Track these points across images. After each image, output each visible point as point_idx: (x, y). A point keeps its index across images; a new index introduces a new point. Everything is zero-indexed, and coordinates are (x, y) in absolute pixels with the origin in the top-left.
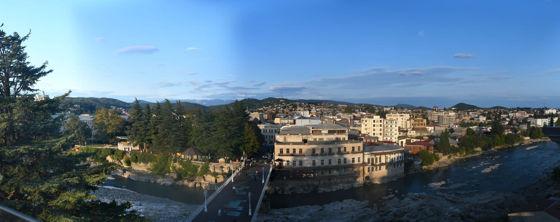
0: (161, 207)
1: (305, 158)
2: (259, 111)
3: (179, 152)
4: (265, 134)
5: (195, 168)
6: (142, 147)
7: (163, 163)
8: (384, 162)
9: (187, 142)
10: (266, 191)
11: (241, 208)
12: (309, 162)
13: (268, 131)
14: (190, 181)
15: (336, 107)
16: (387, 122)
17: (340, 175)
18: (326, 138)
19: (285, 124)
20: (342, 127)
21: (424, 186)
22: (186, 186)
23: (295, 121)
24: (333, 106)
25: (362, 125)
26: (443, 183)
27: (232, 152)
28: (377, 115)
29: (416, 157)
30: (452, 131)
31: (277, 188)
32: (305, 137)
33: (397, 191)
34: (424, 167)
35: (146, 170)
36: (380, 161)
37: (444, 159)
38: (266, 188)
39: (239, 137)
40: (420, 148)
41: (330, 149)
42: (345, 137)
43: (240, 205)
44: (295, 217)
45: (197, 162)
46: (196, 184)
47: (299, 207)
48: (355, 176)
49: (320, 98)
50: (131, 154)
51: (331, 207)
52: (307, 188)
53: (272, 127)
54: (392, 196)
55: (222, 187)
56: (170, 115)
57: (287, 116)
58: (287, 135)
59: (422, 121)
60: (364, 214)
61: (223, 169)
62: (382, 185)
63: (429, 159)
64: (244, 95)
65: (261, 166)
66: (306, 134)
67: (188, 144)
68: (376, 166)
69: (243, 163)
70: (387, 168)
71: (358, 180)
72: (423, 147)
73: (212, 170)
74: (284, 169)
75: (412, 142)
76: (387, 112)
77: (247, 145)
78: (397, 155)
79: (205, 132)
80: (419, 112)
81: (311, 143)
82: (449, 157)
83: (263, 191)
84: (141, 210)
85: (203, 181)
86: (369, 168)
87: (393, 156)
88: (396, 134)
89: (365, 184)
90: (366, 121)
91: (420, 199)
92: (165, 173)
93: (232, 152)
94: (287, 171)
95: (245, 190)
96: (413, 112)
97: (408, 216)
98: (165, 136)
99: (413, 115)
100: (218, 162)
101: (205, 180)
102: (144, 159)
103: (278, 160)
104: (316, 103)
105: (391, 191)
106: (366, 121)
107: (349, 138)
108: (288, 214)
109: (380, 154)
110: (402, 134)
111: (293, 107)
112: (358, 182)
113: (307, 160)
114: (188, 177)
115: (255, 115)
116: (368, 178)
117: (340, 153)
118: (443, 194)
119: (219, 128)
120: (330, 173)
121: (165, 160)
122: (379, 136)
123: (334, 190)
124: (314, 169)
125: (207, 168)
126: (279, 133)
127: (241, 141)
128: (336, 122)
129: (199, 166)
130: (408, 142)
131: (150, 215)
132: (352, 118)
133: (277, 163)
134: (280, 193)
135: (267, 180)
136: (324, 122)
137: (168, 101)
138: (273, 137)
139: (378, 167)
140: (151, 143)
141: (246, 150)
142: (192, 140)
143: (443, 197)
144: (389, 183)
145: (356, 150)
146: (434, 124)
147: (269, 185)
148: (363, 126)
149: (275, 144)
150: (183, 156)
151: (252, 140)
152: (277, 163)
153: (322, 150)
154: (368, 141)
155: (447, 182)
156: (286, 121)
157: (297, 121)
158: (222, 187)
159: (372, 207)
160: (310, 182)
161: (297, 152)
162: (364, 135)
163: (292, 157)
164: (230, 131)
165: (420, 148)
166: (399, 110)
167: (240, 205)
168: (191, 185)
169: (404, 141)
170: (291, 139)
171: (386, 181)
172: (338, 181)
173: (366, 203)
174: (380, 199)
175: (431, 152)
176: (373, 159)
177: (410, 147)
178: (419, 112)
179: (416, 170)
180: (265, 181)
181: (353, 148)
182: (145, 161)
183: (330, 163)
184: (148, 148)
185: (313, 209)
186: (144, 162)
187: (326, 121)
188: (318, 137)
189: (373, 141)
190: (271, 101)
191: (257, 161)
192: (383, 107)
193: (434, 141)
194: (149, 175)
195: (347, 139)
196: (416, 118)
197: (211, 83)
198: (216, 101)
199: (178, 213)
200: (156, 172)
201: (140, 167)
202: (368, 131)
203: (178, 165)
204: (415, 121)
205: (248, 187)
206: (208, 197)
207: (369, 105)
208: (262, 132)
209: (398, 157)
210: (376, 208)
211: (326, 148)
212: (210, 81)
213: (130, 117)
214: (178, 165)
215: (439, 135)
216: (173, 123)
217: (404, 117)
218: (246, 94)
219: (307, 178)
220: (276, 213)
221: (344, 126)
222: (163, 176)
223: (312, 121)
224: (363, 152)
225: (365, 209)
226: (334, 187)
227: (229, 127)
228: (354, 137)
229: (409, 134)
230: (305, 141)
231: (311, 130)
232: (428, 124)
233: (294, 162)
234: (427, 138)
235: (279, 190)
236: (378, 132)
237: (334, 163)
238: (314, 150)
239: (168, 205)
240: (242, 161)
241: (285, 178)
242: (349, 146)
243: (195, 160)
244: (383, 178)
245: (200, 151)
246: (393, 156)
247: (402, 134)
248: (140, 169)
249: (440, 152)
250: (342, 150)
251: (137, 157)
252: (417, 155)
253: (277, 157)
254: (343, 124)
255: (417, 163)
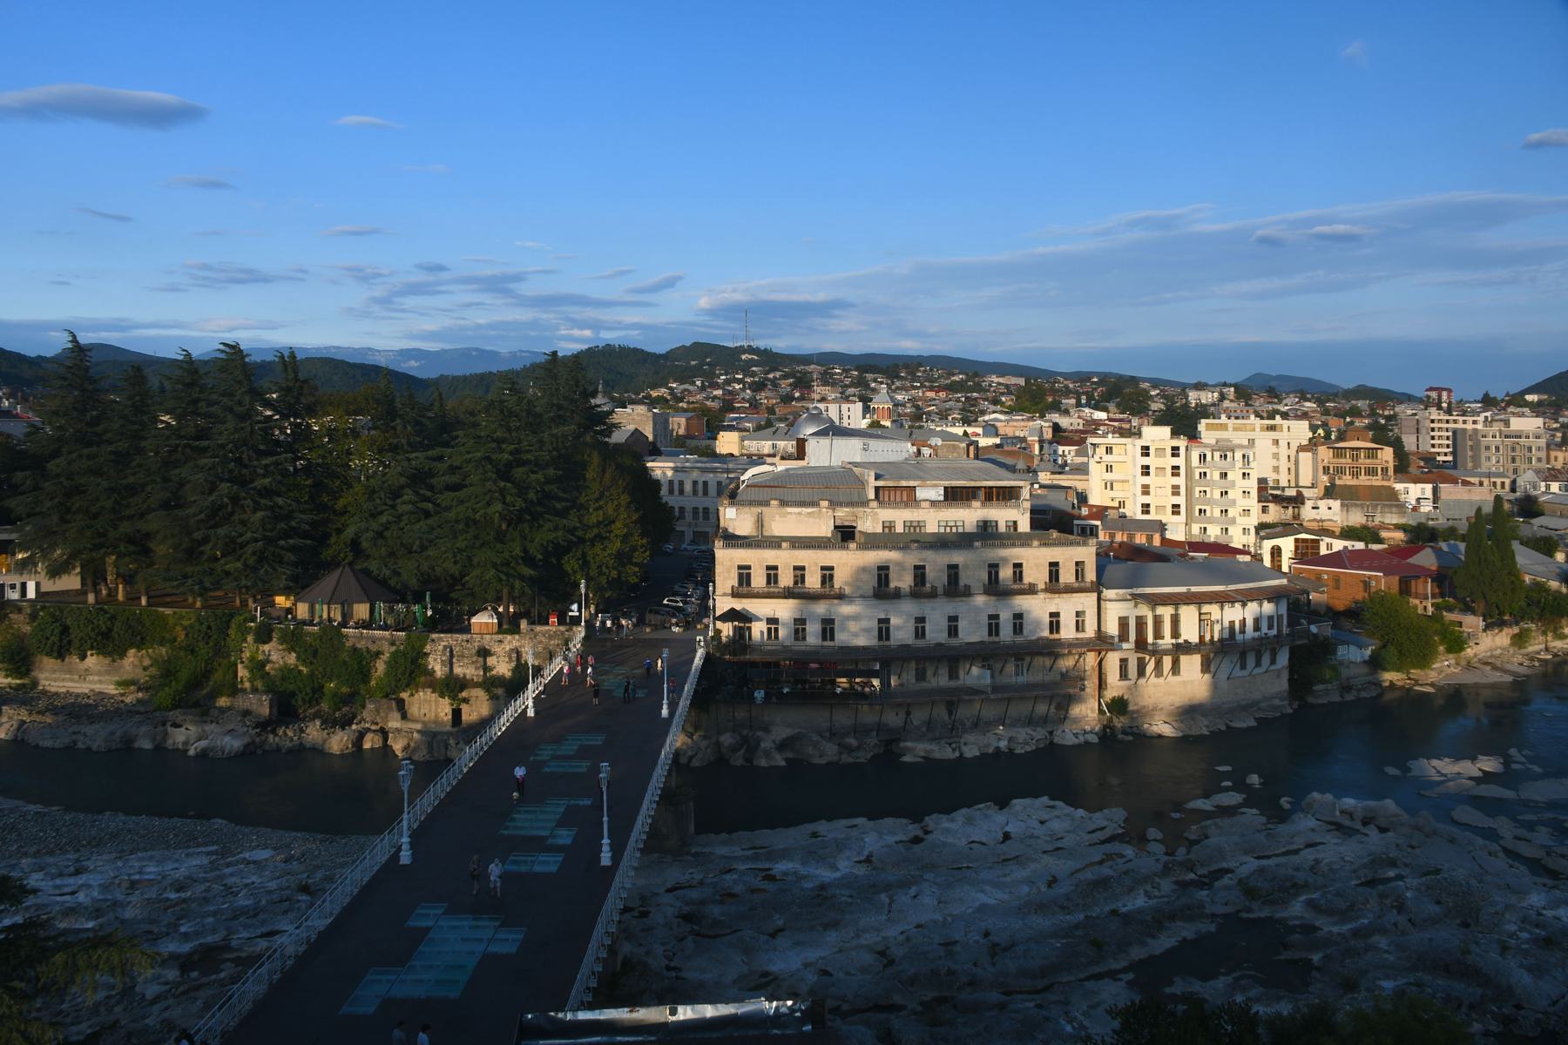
0: (191, 863)
1: (846, 609)
2: (652, 403)
3: (286, 592)
4: (673, 501)
5: (362, 662)
6: (93, 576)
7: (204, 650)
8: (1195, 639)
9: (323, 539)
10: (677, 754)
11: (565, 837)
12: (865, 624)
13: (688, 487)
14: (331, 723)
15: (978, 388)
16: (1203, 458)
17: (996, 688)
18: (934, 520)
19: (759, 459)
20: (1003, 472)
21: (1391, 771)
22: (318, 751)
23: (801, 444)
24: (963, 383)
25: (1093, 466)
26: (1489, 764)
27: (531, 581)
28: (1158, 422)
29: (1347, 624)
30: (1529, 507)
31: (727, 739)
32: (843, 514)
33: (1254, 779)
34: (1389, 677)
35: (111, 689)
36: (1175, 633)
37: (1490, 648)
38: (676, 739)
39: (562, 514)
40: (1366, 584)
41: (953, 569)
42: (1017, 516)
43: (563, 823)
44: (803, 871)
45: (370, 630)
46: (361, 736)
47: (822, 827)
48: (1064, 691)
49: (909, 346)
50: (33, 617)
51: (958, 830)
52: (852, 741)
53: (704, 470)
54: (1232, 798)
55: (482, 742)
56: (246, 416)
57: (769, 424)
58: (766, 504)
59: (1371, 453)
60: (1106, 871)
61: (491, 661)
62: (1184, 742)
63: (1414, 642)
64: (587, 333)
65: (656, 645)
66: (851, 504)
67: (327, 554)
68: (1157, 653)
69: (580, 632)
70: (1206, 667)
71: (1077, 710)
72: (1381, 581)
73: (437, 666)
74: (756, 657)
75: (1323, 551)
76: (1203, 412)
77: (598, 549)
78: (1253, 607)
79: (408, 495)
80: (1357, 411)
81: (872, 542)
82: (1520, 640)
83: (665, 753)
84: (81, 897)
85: (394, 723)
86: (1124, 662)
87: (1234, 614)
88: (1246, 512)
89: (1107, 735)
90: (1109, 450)
91: (1372, 832)
92: (214, 695)
93: (531, 581)
94: (767, 665)
95: (583, 753)
96: (1326, 412)
97: (1311, 904)
98: (216, 516)
99: (1325, 425)
100: (467, 630)
101: (404, 717)
102: (106, 635)
103: (732, 615)
104: (894, 368)
105: (1226, 776)
106: (1109, 450)
107: (1034, 524)
108: (773, 856)
109: (1176, 601)
110: (1275, 513)
111: (794, 386)
112: (1076, 720)
113: (855, 618)
114: (325, 706)
115: (634, 419)
116: (1119, 706)
117: (994, 588)
118: (1487, 822)
119: (474, 478)
120: (953, 675)
121: (215, 637)
122: (1167, 517)
123: (971, 752)
124: (885, 657)
125: (414, 661)
126: (733, 497)
127: (572, 531)
128: (979, 454)
129: (378, 654)
130: (1306, 553)
131: (129, 914)
132: (1048, 434)
133: (727, 629)
134: (738, 760)
135: (684, 703)
136: (926, 451)
137: (234, 352)
138: (711, 516)
139: (1167, 661)
140: (147, 551)
141: (593, 572)
142: (350, 531)
143: (1491, 835)
144: (1211, 737)
145: (1067, 576)
146: (1434, 471)
147: (693, 725)
148: (1096, 471)
149: (718, 544)
150: (302, 610)
151: (619, 528)
152: (727, 629)
153: (919, 572)
154: (1119, 537)
155: (1507, 762)
156: (766, 446)
157: (811, 446)
158: (482, 742)
159: (1142, 840)
160: (868, 715)
161: (813, 581)
162: (1100, 512)
163: (791, 603)
164: (522, 489)
165: (1366, 585)
166: (1259, 403)
167: (563, 823)
168: (338, 742)
169: (1287, 545)
170: (787, 522)
171: (1202, 727)
172: (989, 712)
173: (1111, 818)
174: (1178, 806)
175: (1424, 603)
176: (1141, 623)
177: (1318, 576)
178: (1357, 411)
179: (1348, 688)
180: (674, 708)
181: (1054, 567)
182: (109, 643)
183: (953, 631)
184: (129, 579)
185: (879, 837)
186: (102, 651)
187: (935, 448)
188: (900, 517)
189: (1140, 539)
190: (702, 360)
191: (641, 622)
192: (1184, 388)
193: (1438, 551)
194: (131, 711)
195: (1024, 526)
196: (1341, 438)
197: (444, 276)
198: (465, 353)
199: (273, 885)
200: (165, 695)
201: (88, 677)
202: (1118, 493)
203: (277, 655)
204: (1339, 452)
205: (597, 740)
206: (418, 789)
207: (1121, 377)
208: (664, 491)
209: (1257, 621)
210: (1158, 849)
211: (934, 564)
212: (441, 268)
213: (35, 429)
214: (277, 655)
215: (1463, 528)
216: (261, 454)
217: (1282, 436)
218: (596, 326)
219: (854, 696)
220: (722, 851)
221: (1012, 469)
222: (203, 710)
223: (873, 443)
224: (1098, 587)
225: (1109, 848)
226: (970, 738)
227: (518, 472)
228: (1055, 521)
229: (1307, 512)
230: (846, 534)
231: (872, 483)
232: (1402, 468)
233: (800, 622)
234: (1400, 535)
235: (734, 749)
236: (1161, 499)
237: (972, 633)
238: (883, 572)
239: (224, 853)
240: (576, 621)
241: (759, 695)
242: (1035, 560)
243: (366, 625)
244: (1189, 712)
245: (383, 583)
246: (1234, 614)
247: (1275, 513)
248: (82, 688)
249: (1468, 609)
250: (1006, 573)
251: (65, 630)
252: (1354, 613)
253: (723, 604)
254: (1009, 461)
255: (1353, 654)
